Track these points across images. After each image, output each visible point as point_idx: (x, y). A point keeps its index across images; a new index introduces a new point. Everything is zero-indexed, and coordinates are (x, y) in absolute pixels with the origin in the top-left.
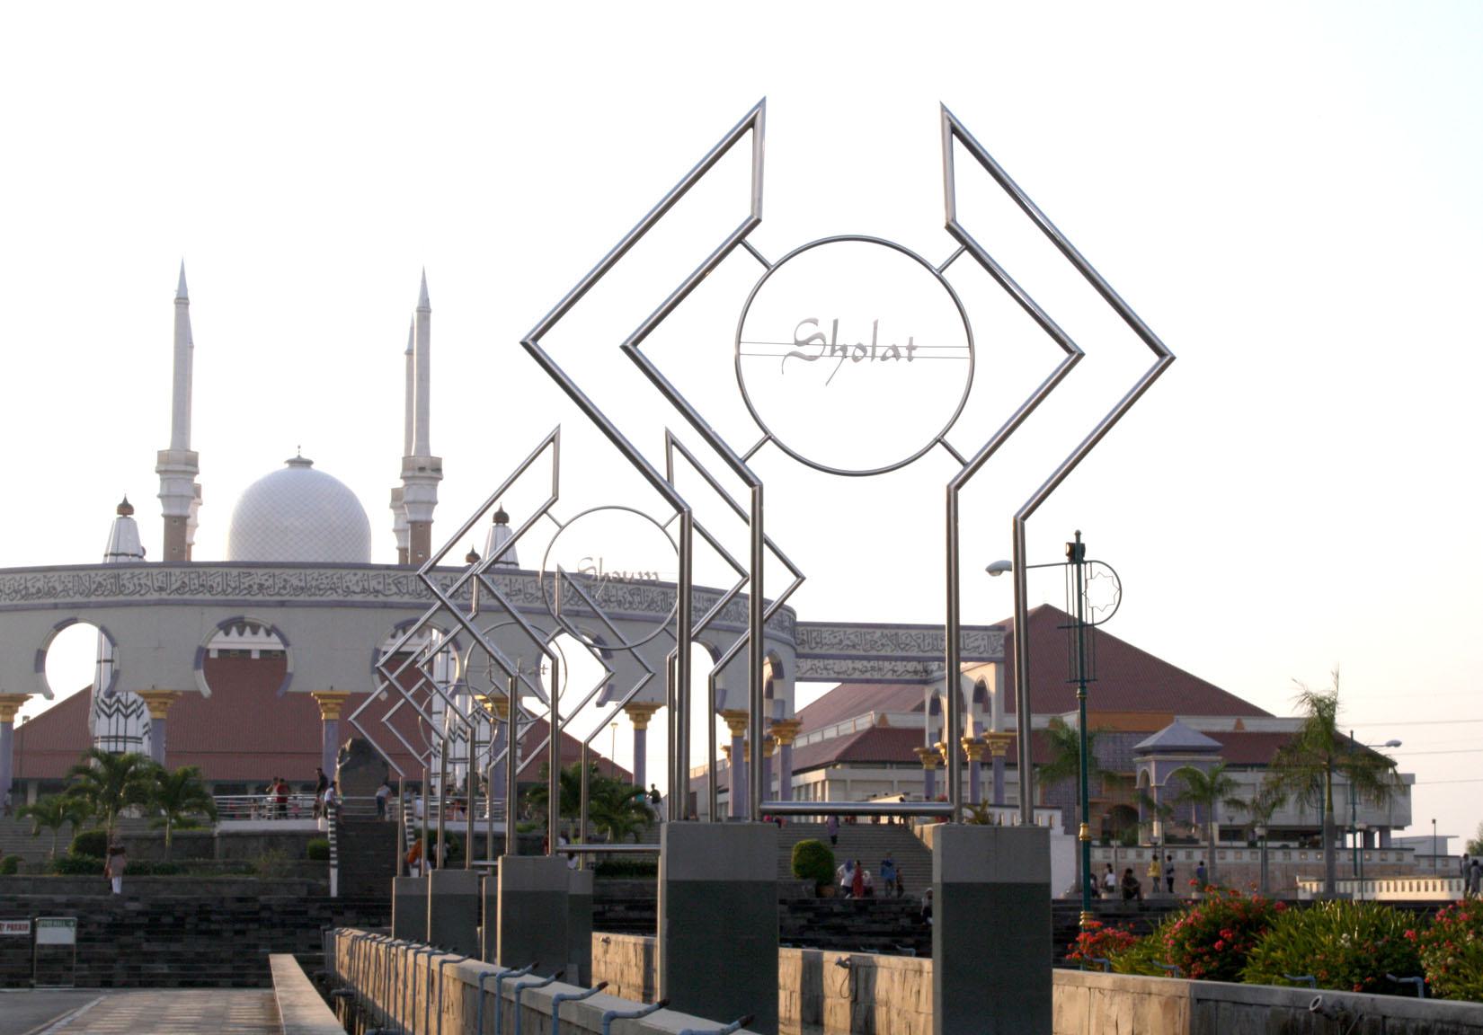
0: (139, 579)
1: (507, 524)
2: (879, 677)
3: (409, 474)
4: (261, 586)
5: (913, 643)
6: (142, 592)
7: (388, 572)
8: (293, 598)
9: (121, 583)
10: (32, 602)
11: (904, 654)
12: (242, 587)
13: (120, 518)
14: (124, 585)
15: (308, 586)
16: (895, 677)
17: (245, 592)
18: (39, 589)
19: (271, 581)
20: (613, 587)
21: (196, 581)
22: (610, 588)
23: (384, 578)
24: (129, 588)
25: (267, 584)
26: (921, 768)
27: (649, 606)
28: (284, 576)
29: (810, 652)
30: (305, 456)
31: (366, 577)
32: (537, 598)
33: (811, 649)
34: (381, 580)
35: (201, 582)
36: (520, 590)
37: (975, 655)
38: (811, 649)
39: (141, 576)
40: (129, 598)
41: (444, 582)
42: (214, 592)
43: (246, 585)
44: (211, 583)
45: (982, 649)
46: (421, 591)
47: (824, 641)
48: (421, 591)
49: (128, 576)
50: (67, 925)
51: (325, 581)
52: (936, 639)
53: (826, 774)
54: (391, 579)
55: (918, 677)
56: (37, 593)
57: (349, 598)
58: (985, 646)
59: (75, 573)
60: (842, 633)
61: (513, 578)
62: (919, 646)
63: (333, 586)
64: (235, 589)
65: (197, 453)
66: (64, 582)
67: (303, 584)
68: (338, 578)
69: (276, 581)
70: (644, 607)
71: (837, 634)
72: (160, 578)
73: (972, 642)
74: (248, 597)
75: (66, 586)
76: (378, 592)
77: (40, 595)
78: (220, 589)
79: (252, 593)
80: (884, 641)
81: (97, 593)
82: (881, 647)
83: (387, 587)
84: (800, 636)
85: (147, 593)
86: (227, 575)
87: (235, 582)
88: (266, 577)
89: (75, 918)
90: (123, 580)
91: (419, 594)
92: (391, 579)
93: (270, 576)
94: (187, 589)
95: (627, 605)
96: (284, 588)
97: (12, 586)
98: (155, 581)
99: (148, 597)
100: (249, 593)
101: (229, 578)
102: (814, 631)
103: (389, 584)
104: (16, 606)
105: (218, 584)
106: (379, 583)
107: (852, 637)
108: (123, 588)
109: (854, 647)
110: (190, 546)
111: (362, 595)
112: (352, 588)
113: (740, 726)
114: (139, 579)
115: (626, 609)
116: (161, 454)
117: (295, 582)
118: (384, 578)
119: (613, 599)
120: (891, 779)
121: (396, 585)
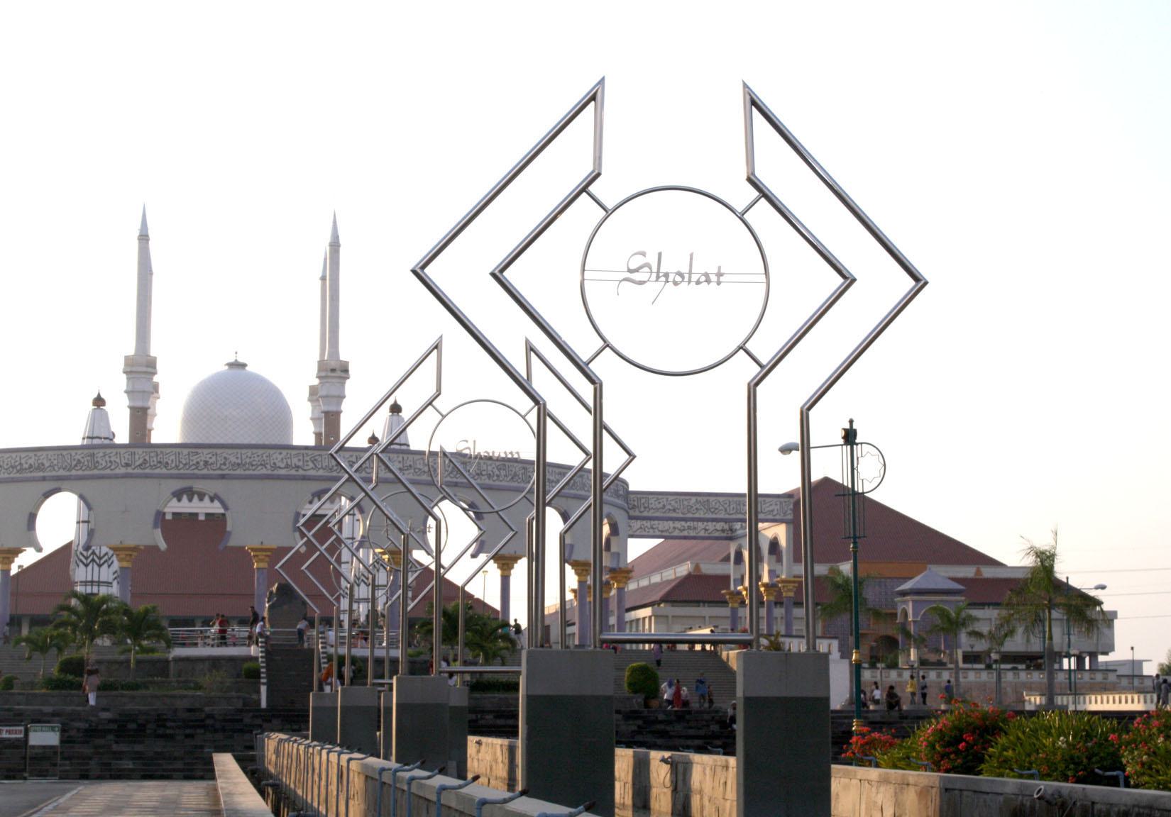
0: (110, 457)
1: (400, 414)
2: (694, 534)
3: (323, 374)
4: (206, 462)
5: (721, 508)
6: (112, 467)
7: (306, 451)
8: (232, 472)
9: (96, 460)
10: (25, 475)
11: (714, 516)
12: (191, 463)
13: (95, 409)
14: (98, 462)
15: (243, 462)
16: (707, 535)
17: (193, 467)
18: (31, 465)
19: (214, 459)
20: (484, 463)
21: (155, 459)
22: (482, 464)
23: (303, 457)
24: (102, 464)
25: (211, 461)
26: (728, 606)
27: (512, 478)
28: (225, 455)
29: (640, 514)
30: (241, 360)
31: (289, 456)
32: (424, 472)
33: (641, 512)
34: (301, 458)
35: (159, 460)
36: (410, 466)
37: (770, 517)
38: (641, 512)
39: (111, 455)
40: (102, 472)
41: (351, 459)
42: (169, 467)
43: (194, 462)
44: (167, 460)
45: (775, 512)
46: (333, 466)
47: (651, 506)
48: (333, 466)
49: (101, 454)
50: (53, 730)
51: (257, 459)
52: (739, 505)
53: (653, 611)
54: (309, 457)
55: (725, 535)
56: (30, 468)
57: (275, 472)
58: (778, 510)
59: (59, 452)
60: (665, 500)
61: (405, 456)
62: (726, 510)
63: (263, 463)
64: (185, 465)
65: (155, 358)
66: (50, 460)
67: (239, 461)
68: (267, 457)
69: (218, 458)
70: (508, 479)
71: (661, 501)
72: (126, 456)
73: (767, 507)
74: (196, 471)
75: (52, 462)
76: (298, 467)
77: (31, 470)
78: (173, 465)
79: (199, 468)
80: (698, 506)
81: (76, 468)
82: (695, 511)
83: (305, 464)
84: (632, 502)
85: (116, 468)
86: (179, 454)
87: (185, 459)
88: (210, 456)
89: (59, 725)
90: (97, 457)
91: (331, 469)
92: (309, 457)
93: (213, 455)
94: (148, 465)
95: (495, 478)
96: (225, 464)
97: (9, 463)
98: (123, 459)
99: (117, 471)
100: (197, 468)
101: (181, 456)
102: (643, 498)
103: (307, 461)
104: (13, 478)
105: (172, 461)
106: (299, 460)
107: (673, 503)
108: (97, 465)
109: (674, 510)
110: (150, 431)
111: (285, 470)
112: (278, 464)
113: (584, 573)
114: (110, 457)
115: (494, 481)
116: (127, 358)
117: (233, 459)
118: (303, 457)
119: (484, 473)
120: (703, 615)
121: (313, 462)
